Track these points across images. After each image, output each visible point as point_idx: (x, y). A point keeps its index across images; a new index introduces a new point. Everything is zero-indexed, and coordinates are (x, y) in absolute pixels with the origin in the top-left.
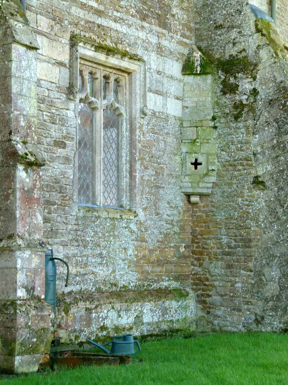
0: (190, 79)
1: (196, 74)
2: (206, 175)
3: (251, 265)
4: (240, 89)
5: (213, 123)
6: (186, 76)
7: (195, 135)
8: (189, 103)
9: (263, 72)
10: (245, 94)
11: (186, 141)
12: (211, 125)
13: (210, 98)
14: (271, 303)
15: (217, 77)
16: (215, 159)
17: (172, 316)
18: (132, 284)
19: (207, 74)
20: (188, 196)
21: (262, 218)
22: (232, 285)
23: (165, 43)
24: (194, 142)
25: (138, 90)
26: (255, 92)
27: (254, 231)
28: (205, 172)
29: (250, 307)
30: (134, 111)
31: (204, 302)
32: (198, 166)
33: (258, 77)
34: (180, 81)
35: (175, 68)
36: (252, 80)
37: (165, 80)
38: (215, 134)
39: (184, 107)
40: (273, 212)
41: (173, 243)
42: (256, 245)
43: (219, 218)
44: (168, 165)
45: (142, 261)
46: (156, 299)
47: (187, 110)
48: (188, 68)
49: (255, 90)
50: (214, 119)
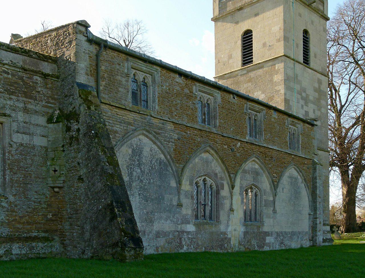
0: (51, 125)
1: (53, 123)
2: (60, 176)
3: (78, 223)
4: (72, 129)
5: (62, 148)
6: (49, 124)
7: (54, 155)
8: (50, 139)
9: (82, 119)
10: (74, 131)
11: (49, 159)
12: (61, 150)
13: (61, 135)
14: (87, 243)
15: (64, 123)
16: (64, 168)
17: (39, 251)
18: (4, 234)
19: (59, 122)
20: (53, 188)
21: (82, 197)
22: (73, 235)
23: (29, 106)
24: (53, 159)
25: (7, 132)
26: (78, 130)
27: (79, 205)
28: (59, 175)
29: (80, 245)
30: (4, 143)
31: (63, 244)
32: (56, 172)
33: (80, 121)
34: (46, 127)
35: (42, 120)
36: (77, 123)
37: (32, 127)
38: (63, 154)
39: (49, 141)
40: (87, 195)
41: (41, 213)
42: (81, 213)
43: (67, 199)
44: (35, 172)
45: (13, 223)
46: (23, 242)
47: (50, 143)
48: (50, 121)
49: (79, 128)
50: (63, 146)
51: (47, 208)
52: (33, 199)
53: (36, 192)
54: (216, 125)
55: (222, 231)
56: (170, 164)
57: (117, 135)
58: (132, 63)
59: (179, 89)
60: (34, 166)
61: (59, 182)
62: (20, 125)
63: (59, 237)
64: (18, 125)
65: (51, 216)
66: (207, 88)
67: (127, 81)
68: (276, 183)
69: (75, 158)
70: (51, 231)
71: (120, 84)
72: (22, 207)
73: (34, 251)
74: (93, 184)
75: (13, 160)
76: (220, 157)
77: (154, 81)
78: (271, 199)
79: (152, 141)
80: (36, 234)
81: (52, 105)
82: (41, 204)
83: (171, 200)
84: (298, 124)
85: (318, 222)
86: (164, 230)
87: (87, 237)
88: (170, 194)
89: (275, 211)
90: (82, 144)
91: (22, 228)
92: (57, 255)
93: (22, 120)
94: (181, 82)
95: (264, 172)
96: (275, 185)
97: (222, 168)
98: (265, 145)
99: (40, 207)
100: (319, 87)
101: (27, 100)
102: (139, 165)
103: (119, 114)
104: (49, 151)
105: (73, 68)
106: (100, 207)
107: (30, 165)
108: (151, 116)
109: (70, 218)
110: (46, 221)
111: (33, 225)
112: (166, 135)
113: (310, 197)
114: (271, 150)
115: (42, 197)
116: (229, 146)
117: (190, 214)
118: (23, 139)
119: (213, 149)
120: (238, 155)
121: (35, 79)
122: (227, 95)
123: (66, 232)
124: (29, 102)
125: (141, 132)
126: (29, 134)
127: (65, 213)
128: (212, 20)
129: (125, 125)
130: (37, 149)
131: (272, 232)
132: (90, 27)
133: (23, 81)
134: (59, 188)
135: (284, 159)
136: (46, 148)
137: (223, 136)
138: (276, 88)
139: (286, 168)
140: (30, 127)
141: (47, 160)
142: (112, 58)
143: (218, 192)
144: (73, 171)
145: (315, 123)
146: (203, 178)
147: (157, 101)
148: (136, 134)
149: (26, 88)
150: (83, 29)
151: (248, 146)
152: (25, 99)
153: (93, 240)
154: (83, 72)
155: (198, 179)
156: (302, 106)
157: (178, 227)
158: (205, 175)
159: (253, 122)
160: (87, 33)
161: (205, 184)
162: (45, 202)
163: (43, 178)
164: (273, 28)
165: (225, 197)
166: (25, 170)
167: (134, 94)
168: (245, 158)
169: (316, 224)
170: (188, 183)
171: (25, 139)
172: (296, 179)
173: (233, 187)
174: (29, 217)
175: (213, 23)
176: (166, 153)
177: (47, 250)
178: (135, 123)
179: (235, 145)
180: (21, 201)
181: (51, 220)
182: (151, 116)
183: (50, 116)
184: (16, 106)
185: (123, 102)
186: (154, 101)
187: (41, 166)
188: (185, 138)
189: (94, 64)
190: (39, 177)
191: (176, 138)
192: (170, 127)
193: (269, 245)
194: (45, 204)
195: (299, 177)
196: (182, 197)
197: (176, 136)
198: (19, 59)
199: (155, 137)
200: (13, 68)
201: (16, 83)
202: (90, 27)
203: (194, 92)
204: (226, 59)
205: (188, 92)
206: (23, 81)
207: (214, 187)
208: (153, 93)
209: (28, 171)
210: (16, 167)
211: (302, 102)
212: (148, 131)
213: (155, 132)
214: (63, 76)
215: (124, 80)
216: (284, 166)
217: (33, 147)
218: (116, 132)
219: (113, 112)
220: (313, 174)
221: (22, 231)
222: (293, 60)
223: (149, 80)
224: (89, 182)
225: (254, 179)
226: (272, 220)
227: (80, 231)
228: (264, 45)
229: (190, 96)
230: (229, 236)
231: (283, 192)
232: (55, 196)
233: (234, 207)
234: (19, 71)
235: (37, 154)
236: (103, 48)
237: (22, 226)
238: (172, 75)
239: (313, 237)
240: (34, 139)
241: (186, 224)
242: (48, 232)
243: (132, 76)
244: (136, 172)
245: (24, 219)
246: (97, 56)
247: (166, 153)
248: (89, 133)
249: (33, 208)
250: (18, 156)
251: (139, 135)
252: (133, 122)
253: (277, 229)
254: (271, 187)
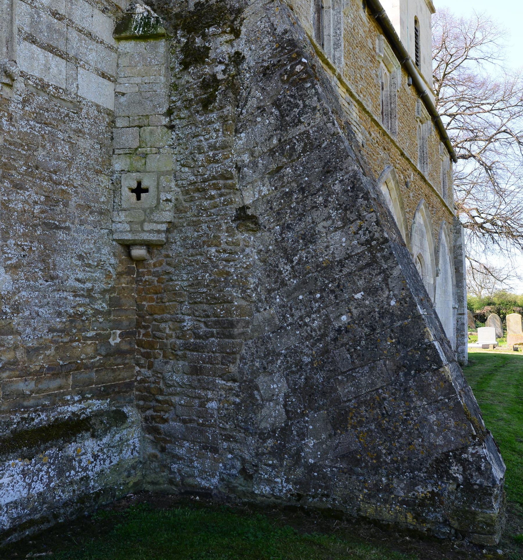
3: (233, 369)
4: (212, 55)
5: (168, 119)
14: (270, 442)
20: (127, 246)
22: (202, 405)
26: (238, 58)
32: (143, 195)
34: (110, 48)
39: (119, 94)
40: (272, 271)
41: (93, 330)
44: (80, 190)
47: (122, 99)
48: (122, 28)
50: (169, 113)
51: (109, 313)
52: (71, 283)
53: (80, 257)
54: (395, 129)
60: (77, 168)
61: (155, 227)
62: (39, 16)
63: (138, 407)
64: (32, 17)
65: (118, 340)
69: (224, 146)
70: (117, 390)
72: (37, 314)
73: (73, 472)
74: (309, 238)
75: (11, 137)
80: (74, 408)
82: (93, 299)
87: (271, 420)
90: (252, 103)
91: (32, 392)
92: (133, 471)
99: (90, 312)
104: (118, 125)
106: (344, 318)
107: (66, 161)
109: (196, 348)
110: (105, 356)
111: (67, 376)
113: (454, 279)
115: (97, 274)
127: (167, 331)
130: (87, 114)
134: (149, 246)
136: (112, 117)
140: (70, 36)
141: (111, 153)
153: (302, 435)
162: (104, 292)
163: (101, 213)
166: (51, 179)
171: (55, 71)
174: (57, 349)
177: (107, 462)
180: (34, 289)
181: (118, 352)
183: (123, 18)
186: (337, 45)
187: (98, 172)
190: (89, 207)
209: (60, 184)
210: (21, 163)
217: (77, 105)
220: (456, 241)
221: (31, 402)
227: (238, 396)
232: (129, 272)
235: (86, 130)
237: (32, 385)
240: (79, 76)
242: (108, 394)
245: (41, 357)
248: (285, 65)
249: (70, 316)
250: (32, 123)
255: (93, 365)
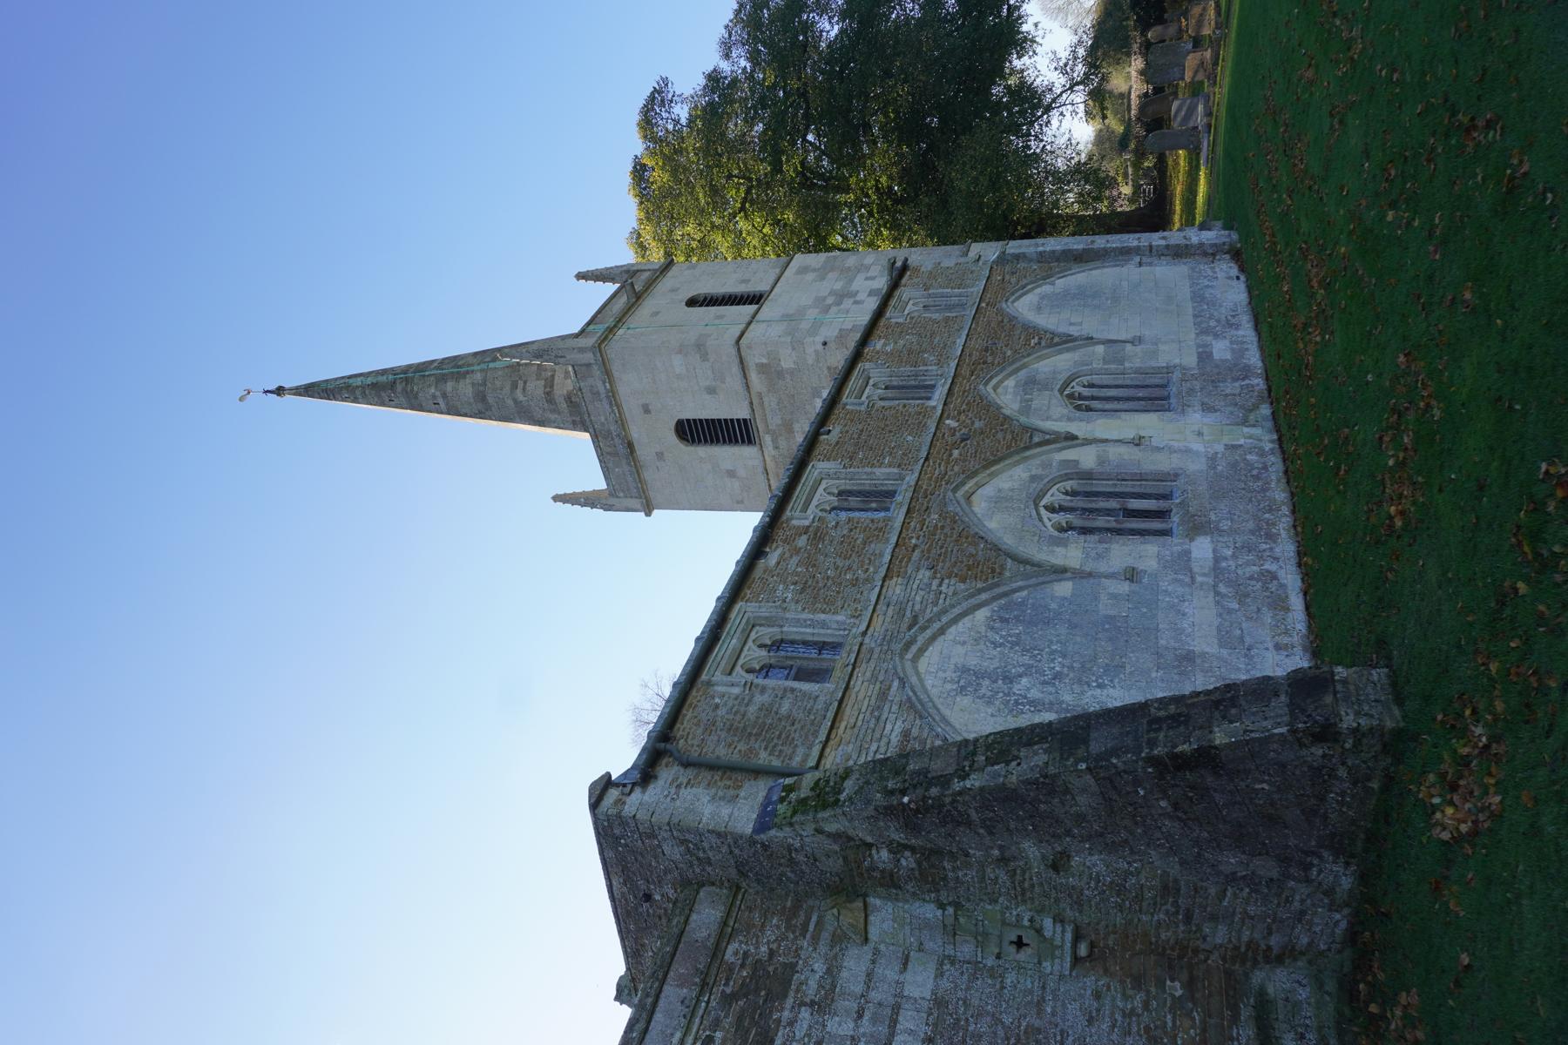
2: (1039, 931)
3: (1213, 891)
9: (862, 833)
20: (1076, 960)
22: (1252, 918)
26: (897, 849)
29: (1297, 897)
34: (876, 952)
55: (1204, 467)
56: (1005, 594)
57: (915, 732)
58: (714, 672)
59: (795, 560)
65: (1177, 984)
66: (801, 492)
67: (763, 690)
68: (1056, 340)
71: (769, 711)
74: (1080, 818)
76: (985, 467)
77: (770, 622)
78: (1100, 349)
79: (933, 638)
81: (814, 919)
82: (1133, 1012)
83: (1114, 596)
84: (900, 298)
85: (1163, 242)
86: (1216, 623)
88: (1096, 599)
89: (1137, 341)
93: (852, 1025)
94: (779, 551)
95: (1024, 366)
96: (1062, 342)
97: (1017, 463)
98: (953, 364)
100: (814, 270)
101: (792, 994)
102: (1009, 679)
103: (852, 721)
105: (714, 840)
108: (864, 633)
109: (1188, 918)
110: (1195, 1004)
112: (918, 599)
113: (1091, 265)
114: (967, 351)
116: (955, 445)
117: (1156, 549)
118: (911, 1032)
119: (963, 483)
120: (977, 424)
121: (732, 959)
122: (820, 448)
123: (1239, 939)
124: (797, 991)
125: (908, 664)
126: (896, 1009)
128: (648, 514)
129: (886, 708)
131: (1199, 346)
132: (608, 775)
133: (734, 997)
134: (1077, 938)
135: (989, 322)
137: (927, 459)
138: (810, 362)
139: (1012, 319)
142: (698, 725)
143: (1088, 476)
144: (1026, 885)
145: (899, 264)
146: (1043, 511)
147: (823, 616)
148: (914, 680)
149: (757, 991)
150: (613, 794)
151: (956, 401)
152: (790, 1001)
154: (725, 811)
155: (1049, 524)
156: (856, 302)
157: (1202, 584)
158: (1036, 506)
159: (890, 393)
160: (624, 785)
161: (1062, 509)
164: (678, 371)
165: (1098, 457)
167: (803, 675)
168: (989, 409)
169: (1167, 246)
170: (1060, 550)
172: (1043, 298)
173: (1071, 437)
175: (656, 512)
176: (973, 601)
178: (881, 678)
179: (953, 431)
181: (1190, 985)
182: (864, 633)
184: (808, 1035)
185: (820, 706)
186: (824, 625)
188: (929, 551)
189: (707, 775)
191: (928, 573)
192: (896, 589)
193: (1240, 353)
194: (1132, 998)
195: (1038, 291)
196: (1102, 567)
197: (924, 574)
198: (673, 994)
199: (923, 629)
200: (697, 1021)
201: (740, 1019)
202: (608, 775)
203: (807, 523)
204: (737, 484)
205: (805, 537)
206: (734, 997)
207: (1069, 485)
208: (802, 623)
211: (847, 303)
212: (908, 645)
213: (910, 628)
214: (733, 872)
215: (759, 699)
216: (1009, 325)
217: (939, 1002)
218: (906, 734)
219: (847, 737)
222: (749, 323)
223: (766, 633)
224: (1068, 833)
225: (1046, 386)
226: (1162, 347)
228: (711, 391)
229: (817, 534)
230: (1220, 448)
231: (1081, 324)
233: (1130, 434)
234: (708, 1002)
236: (668, 746)
238: (758, 572)
239: (1205, 254)
241: (1189, 560)
243: (750, 677)
244: (1028, 689)
246: (687, 765)
247: (973, 601)
251: (918, 674)
252: (878, 685)
253: (1191, 336)
254: (1068, 350)
255: (1203, 1022)
